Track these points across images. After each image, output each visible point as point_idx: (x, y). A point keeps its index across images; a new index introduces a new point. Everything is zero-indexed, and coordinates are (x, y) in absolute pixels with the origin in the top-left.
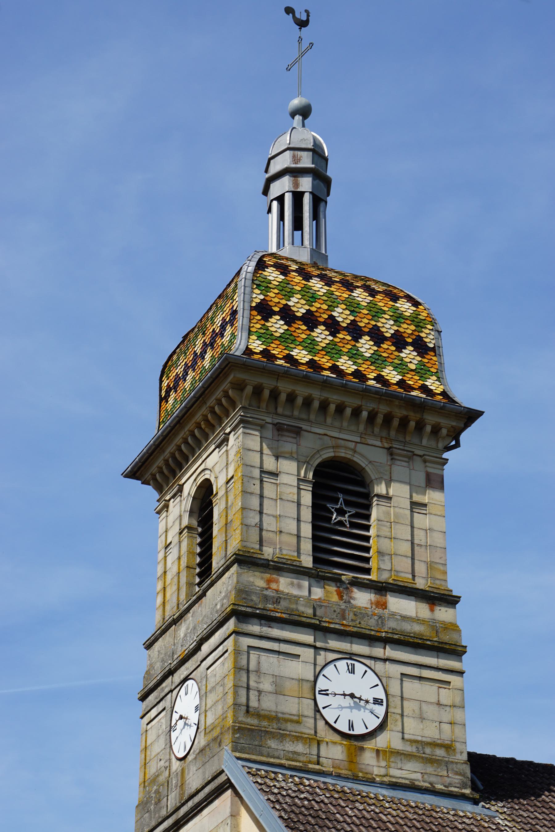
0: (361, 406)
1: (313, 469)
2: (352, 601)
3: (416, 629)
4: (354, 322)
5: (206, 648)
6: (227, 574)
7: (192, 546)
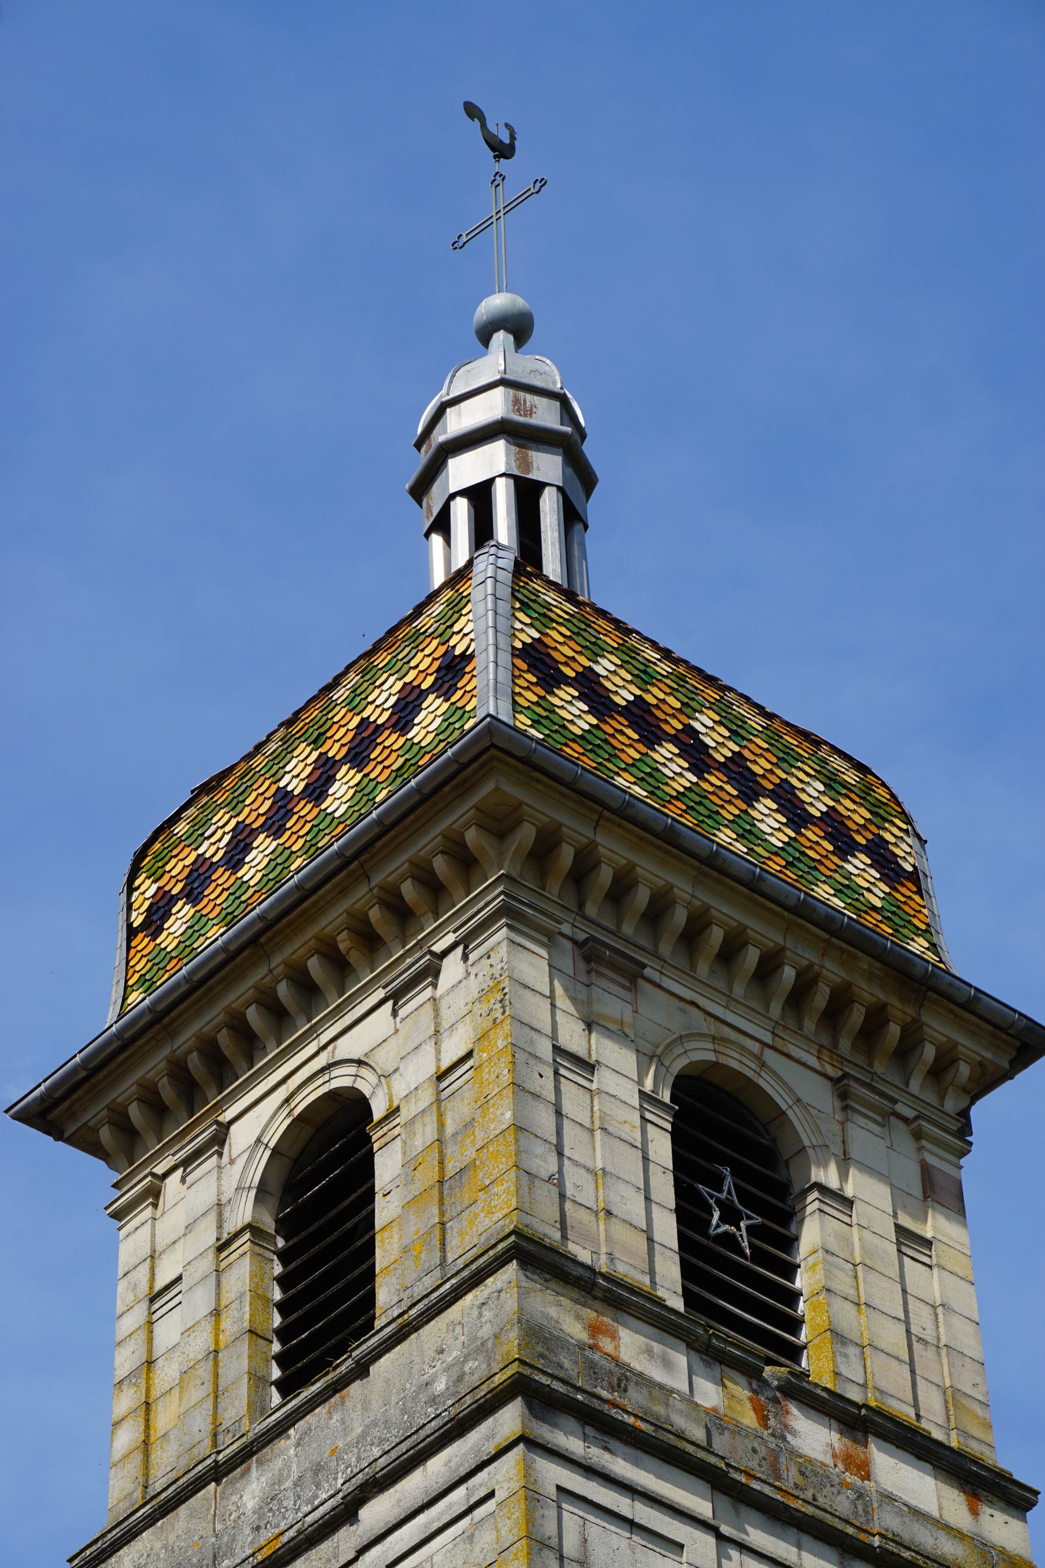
0: (783, 949)
1: (670, 1080)
2: (789, 1437)
3: (945, 1550)
4: (737, 758)
5: (376, 1512)
6: (469, 1297)
7: (262, 1279)
